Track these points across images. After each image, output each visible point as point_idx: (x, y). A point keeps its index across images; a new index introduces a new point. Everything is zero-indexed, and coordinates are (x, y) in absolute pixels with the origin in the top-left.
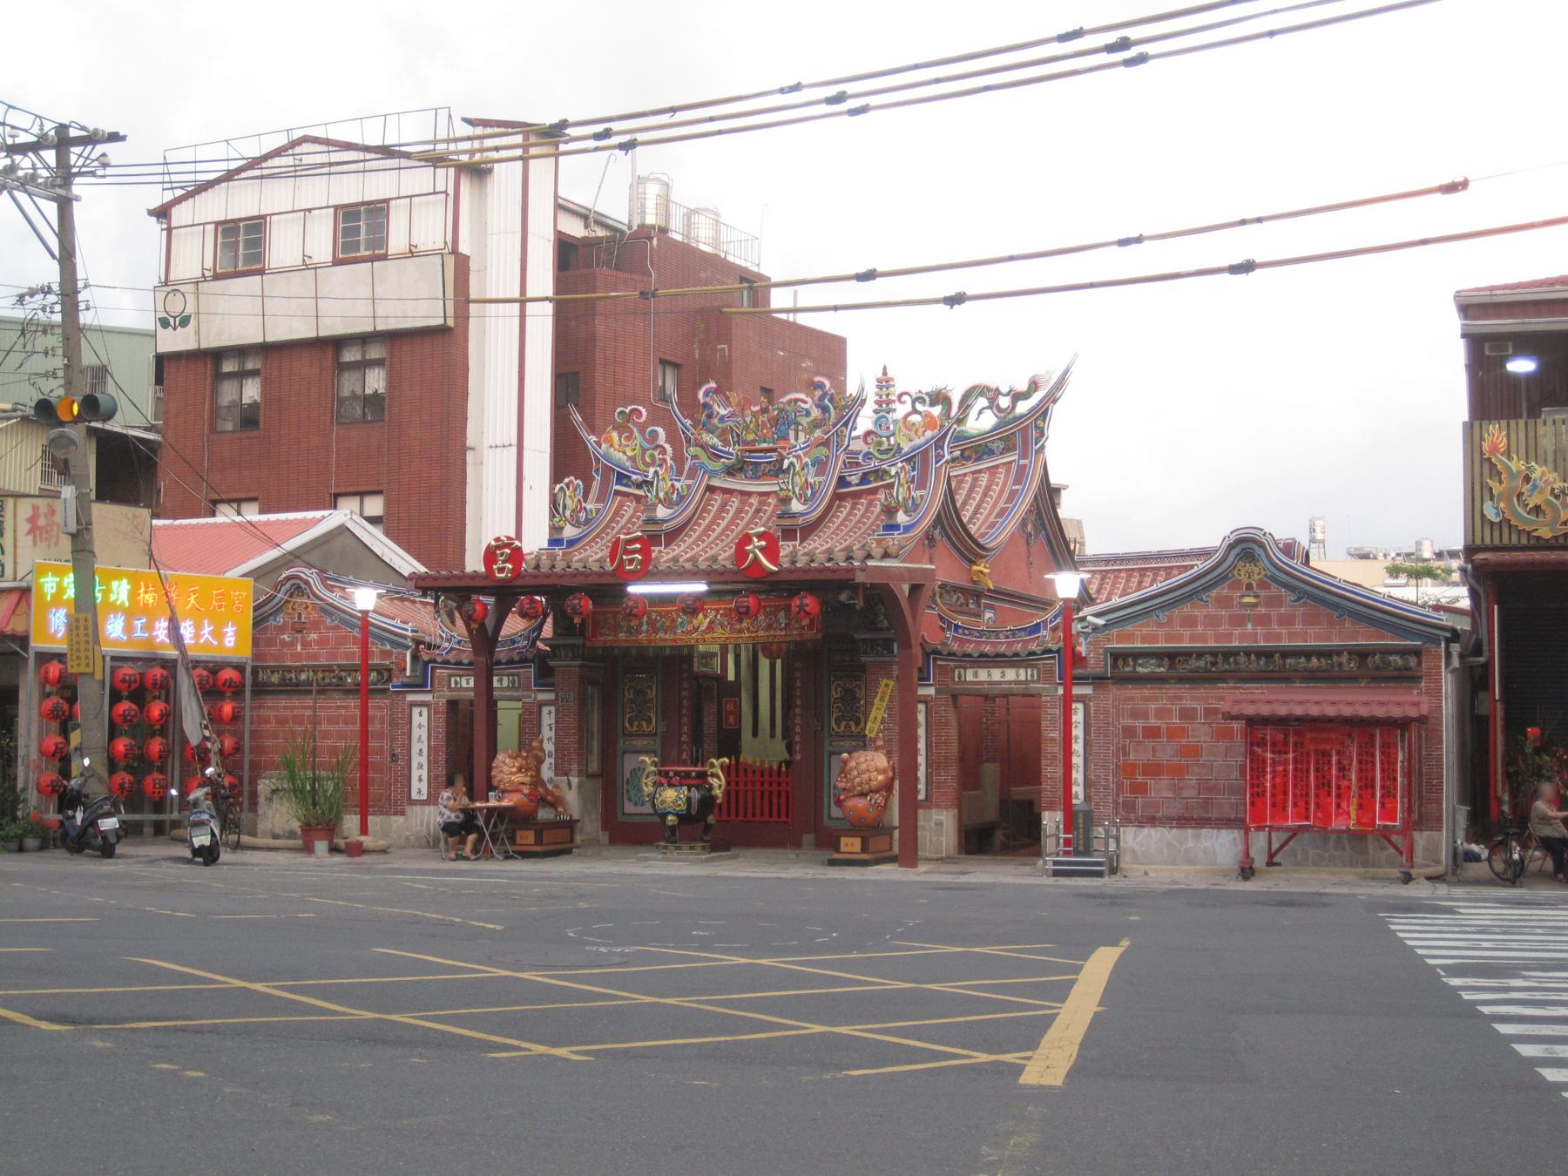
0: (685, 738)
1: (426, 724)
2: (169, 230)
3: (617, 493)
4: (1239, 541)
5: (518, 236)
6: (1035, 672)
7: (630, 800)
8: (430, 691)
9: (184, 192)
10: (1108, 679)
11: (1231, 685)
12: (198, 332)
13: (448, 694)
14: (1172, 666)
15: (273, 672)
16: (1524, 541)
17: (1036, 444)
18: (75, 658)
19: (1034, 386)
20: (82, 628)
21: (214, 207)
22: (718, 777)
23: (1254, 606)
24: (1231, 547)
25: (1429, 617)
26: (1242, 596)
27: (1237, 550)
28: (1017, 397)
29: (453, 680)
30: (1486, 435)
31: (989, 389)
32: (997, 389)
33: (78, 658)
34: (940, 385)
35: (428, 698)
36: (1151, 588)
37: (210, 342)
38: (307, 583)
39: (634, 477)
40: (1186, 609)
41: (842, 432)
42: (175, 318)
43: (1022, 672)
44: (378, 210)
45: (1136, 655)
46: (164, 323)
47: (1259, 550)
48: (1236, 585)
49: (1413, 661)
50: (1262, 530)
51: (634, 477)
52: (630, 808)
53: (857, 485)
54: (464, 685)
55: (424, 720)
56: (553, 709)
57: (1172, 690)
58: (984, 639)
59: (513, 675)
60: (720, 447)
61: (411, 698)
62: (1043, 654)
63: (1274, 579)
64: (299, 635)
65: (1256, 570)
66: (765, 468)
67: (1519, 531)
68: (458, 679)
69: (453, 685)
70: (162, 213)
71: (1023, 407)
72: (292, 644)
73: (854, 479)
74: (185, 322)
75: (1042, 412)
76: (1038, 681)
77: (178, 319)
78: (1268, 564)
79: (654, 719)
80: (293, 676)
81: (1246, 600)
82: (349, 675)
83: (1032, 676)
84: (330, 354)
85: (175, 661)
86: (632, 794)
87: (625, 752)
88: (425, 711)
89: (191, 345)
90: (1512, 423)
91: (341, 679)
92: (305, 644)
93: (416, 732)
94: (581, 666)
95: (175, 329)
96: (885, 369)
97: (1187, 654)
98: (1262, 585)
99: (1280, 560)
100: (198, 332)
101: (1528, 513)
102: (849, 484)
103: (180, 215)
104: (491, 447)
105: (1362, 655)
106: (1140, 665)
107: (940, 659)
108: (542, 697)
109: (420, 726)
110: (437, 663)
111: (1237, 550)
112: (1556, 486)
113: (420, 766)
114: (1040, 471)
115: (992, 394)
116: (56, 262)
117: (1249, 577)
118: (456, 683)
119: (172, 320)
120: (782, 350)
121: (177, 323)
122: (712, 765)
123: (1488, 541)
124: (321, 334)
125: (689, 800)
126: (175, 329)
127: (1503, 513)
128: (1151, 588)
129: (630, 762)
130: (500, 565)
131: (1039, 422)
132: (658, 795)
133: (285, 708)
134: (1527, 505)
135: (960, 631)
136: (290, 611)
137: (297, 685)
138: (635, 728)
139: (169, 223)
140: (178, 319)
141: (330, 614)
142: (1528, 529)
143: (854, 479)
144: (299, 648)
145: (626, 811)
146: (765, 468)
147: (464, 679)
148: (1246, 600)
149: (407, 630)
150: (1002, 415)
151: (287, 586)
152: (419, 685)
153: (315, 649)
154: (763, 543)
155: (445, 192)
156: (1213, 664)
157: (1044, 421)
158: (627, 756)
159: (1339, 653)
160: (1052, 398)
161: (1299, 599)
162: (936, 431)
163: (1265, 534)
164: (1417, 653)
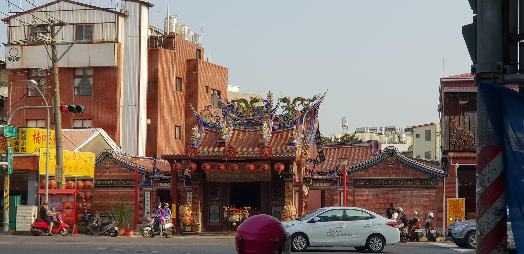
0: (229, 201)
1: (150, 197)
2: (10, 27)
3: (205, 130)
4: (389, 150)
5: (138, 38)
6: (332, 184)
7: (211, 218)
8: (151, 187)
9: (16, 14)
10: (352, 186)
11: (386, 188)
12: (23, 63)
13: (157, 188)
14: (370, 183)
15: (98, 181)
16: (461, 150)
17: (316, 115)
18: (57, 178)
19: (315, 98)
20: (60, 169)
21: (27, 19)
22: (246, 212)
23: (393, 167)
24: (387, 151)
25: (439, 171)
26: (389, 165)
27: (388, 152)
28: (311, 101)
29: (158, 183)
30: (451, 121)
31: (302, 99)
32: (304, 99)
33: (58, 178)
34: (287, 96)
35: (151, 189)
36: (364, 162)
37: (28, 65)
38: (111, 154)
39: (210, 125)
40: (374, 168)
41: (273, 115)
42: (14, 57)
43: (328, 184)
44: (89, 27)
45: (360, 180)
46: (10, 59)
47: (394, 153)
48: (388, 161)
49: (435, 183)
50: (395, 147)
51: (210, 125)
52: (211, 221)
53: (277, 130)
54: (162, 185)
55: (149, 195)
56: (191, 193)
57: (370, 189)
58: (318, 175)
59: (331, 182)
60: (236, 118)
61: (145, 189)
62: (335, 179)
63: (398, 160)
64: (107, 170)
65: (393, 158)
66: (250, 124)
67: (460, 147)
68: (160, 183)
69: (158, 185)
70: (7, 20)
71: (311, 104)
72: (105, 172)
73: (277, 128)
74: (18, 59)
75: (317, 106)
76: (333, 186)
77: (15, 58)
78: (396, 156)
79: (219, 196)
80: (106, 182)
81: (390, 166)
82: (124, 182)
83: (331, 184)
84: (72, 72)
85: (169, 191)
86: (212, 217)
87: (210, 205)
88: (149, 193)
89: (20, 67)
90: (458, 117)
91: (122, 183)
92: (109, 173)
93: (146, 199)
94: (200, 180)
95: (14, 61)
96: (270, 91)
97: (374, 180)
98: (394, 162)
99: (400, 155)
100: (23, 63)
101: (462, 142)
102: (275, 130)
103: (14, 22)
104: (128, 106)
105: (422, 181)
106: (361, 182)
107: (305, 180)
108: (186, 189)
109: (148, 197)
110: (154, 179)
111: (388, 152)
112: (470, 135)
113: (148, 209)
114: (317, 122)
115: (302, 100)
116: (51, 60)
117: (391, 160)
118: (159, 184)
119: (12, 58)
120: (211, 73)
121: (15, 59)
122: (244, 209)
123: (451, 149)
124: (69, 66)
125: (239, 219)
126: (14, 61)
127: (455, 142)
128: (364, 162)
129: (212, 208)
130: (190, 153)
131: (317, 109)
132: (230, 217)
133: (102, 192)
134: (462, 140)
135: (322, 174)
136: (104, 162)
137: (107, 185)
138: (213, 198)
139: (10, 24)
140: (15, 58)
141: (118, 164)
142: (462, 146)
143: (277, 128)
144: (107, 174)
145: (210, 222)
146: (250, 124)
147: (162, 183)
148: (390, 166)
149: (145, 169)
150: (306, 106)
151: (104, 155)
152: (147, 185)
153: (113, 174)
154: (268, 149)
155: (115, 23)
156: (381, 183)
157: (318, 108)
158: (210, 206)
159: (416, 180)
160: (320, 102)
161: (405, 166)
162: (300, 116)
163: (395, 148)
164: (436, 181)
